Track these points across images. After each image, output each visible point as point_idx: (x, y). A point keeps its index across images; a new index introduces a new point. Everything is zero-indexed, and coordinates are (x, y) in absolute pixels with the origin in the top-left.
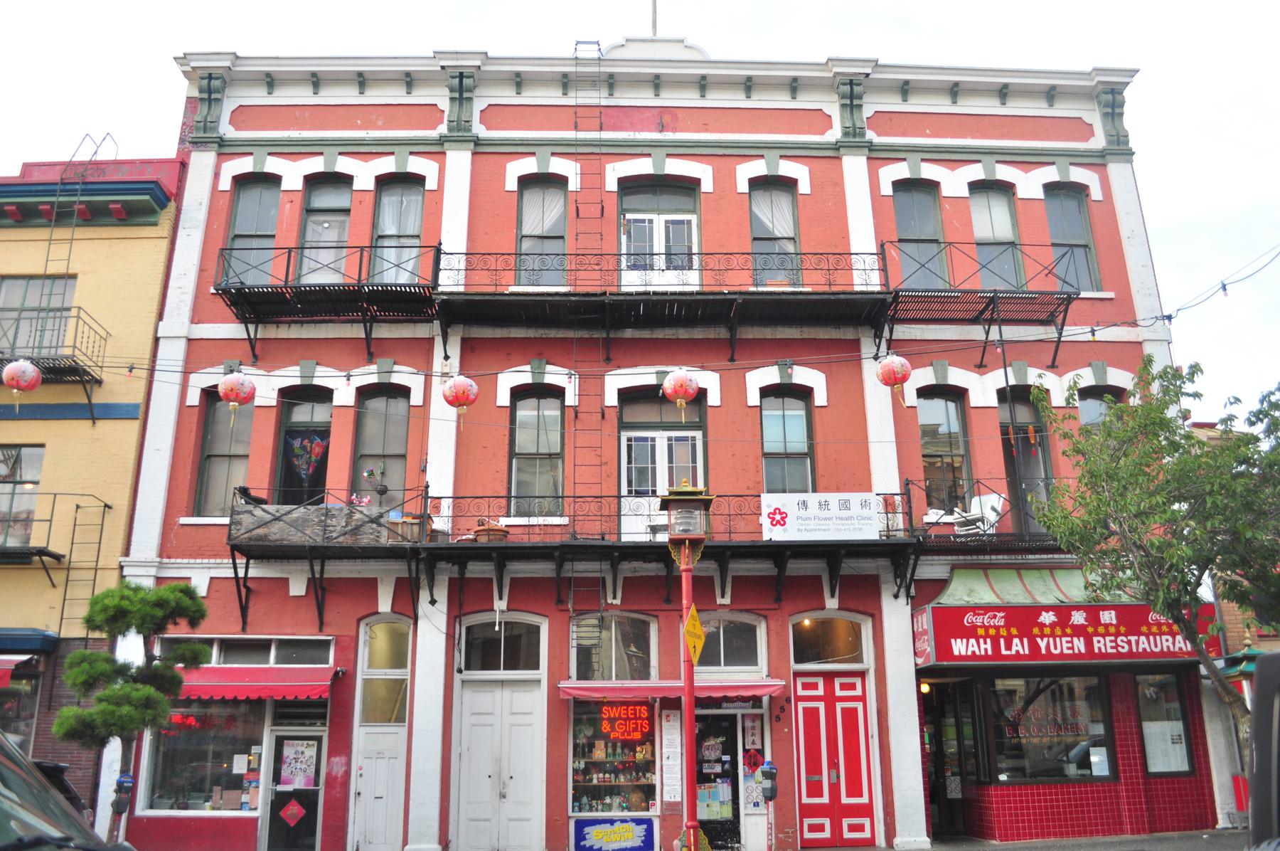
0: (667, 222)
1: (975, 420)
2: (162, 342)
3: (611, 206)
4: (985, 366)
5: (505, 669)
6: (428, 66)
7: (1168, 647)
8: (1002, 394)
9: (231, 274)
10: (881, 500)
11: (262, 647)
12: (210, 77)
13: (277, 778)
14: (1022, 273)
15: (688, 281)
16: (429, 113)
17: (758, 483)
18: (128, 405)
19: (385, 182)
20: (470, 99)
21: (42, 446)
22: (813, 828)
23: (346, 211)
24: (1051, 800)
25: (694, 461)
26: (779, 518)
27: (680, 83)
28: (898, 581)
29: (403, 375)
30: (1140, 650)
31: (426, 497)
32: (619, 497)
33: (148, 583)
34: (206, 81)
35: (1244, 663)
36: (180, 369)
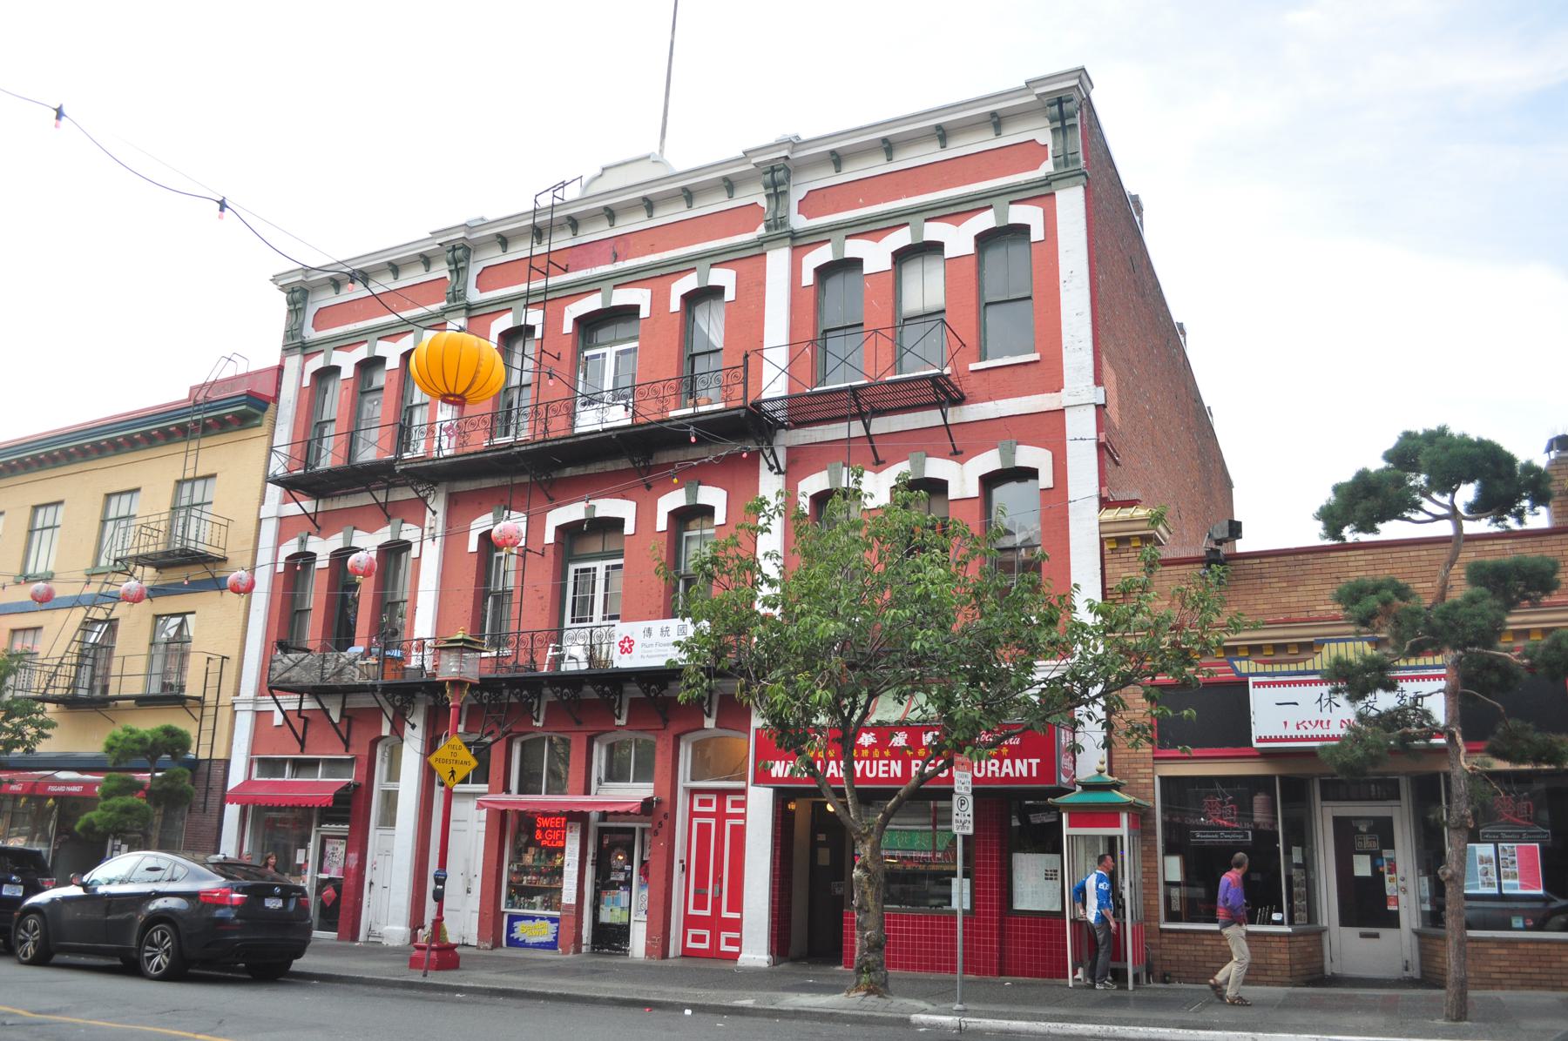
5: (473, 783)
8: (34, 597)
11: (313, 764)
12: (454, 249)
13: (321, 870)
15: (618, 417)
16: (1030, 152)
20: (785, 193)
22: (697, 939)
24: (901, 931)
26: (627, 646)
30: (1003, 775)
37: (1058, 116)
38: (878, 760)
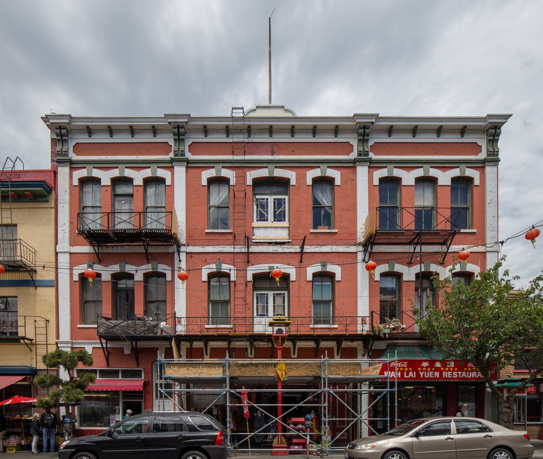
0: (274, 199)
1: (404, 286)
2: (59, 254)
3: (250, 190)
4: (412, 263)
6: (162, 122)
7: (474, 376)
8: (417, 275)
9: (84, 224)
10: (361, 319)
14: (435, 221)
17: (310, 312)
18: (49, 281)
19: (148, 181)
20: (183, 140)
21: (16, 297)
23: (131, 195)
25: (284, 302)
27: (282, 130)
28: (365, 350)
29: (162, 268)
30: (478, 377)
31: (175, 318)
32: (253, 317)
33: (69, 350)
34: (59, 130)
35: (506, 383)
36: (68, 268)
37: (177, 133)
38: (429, 371)
